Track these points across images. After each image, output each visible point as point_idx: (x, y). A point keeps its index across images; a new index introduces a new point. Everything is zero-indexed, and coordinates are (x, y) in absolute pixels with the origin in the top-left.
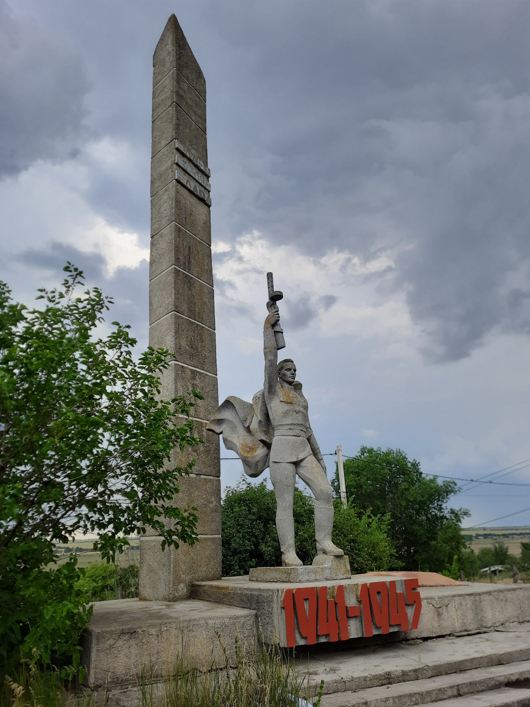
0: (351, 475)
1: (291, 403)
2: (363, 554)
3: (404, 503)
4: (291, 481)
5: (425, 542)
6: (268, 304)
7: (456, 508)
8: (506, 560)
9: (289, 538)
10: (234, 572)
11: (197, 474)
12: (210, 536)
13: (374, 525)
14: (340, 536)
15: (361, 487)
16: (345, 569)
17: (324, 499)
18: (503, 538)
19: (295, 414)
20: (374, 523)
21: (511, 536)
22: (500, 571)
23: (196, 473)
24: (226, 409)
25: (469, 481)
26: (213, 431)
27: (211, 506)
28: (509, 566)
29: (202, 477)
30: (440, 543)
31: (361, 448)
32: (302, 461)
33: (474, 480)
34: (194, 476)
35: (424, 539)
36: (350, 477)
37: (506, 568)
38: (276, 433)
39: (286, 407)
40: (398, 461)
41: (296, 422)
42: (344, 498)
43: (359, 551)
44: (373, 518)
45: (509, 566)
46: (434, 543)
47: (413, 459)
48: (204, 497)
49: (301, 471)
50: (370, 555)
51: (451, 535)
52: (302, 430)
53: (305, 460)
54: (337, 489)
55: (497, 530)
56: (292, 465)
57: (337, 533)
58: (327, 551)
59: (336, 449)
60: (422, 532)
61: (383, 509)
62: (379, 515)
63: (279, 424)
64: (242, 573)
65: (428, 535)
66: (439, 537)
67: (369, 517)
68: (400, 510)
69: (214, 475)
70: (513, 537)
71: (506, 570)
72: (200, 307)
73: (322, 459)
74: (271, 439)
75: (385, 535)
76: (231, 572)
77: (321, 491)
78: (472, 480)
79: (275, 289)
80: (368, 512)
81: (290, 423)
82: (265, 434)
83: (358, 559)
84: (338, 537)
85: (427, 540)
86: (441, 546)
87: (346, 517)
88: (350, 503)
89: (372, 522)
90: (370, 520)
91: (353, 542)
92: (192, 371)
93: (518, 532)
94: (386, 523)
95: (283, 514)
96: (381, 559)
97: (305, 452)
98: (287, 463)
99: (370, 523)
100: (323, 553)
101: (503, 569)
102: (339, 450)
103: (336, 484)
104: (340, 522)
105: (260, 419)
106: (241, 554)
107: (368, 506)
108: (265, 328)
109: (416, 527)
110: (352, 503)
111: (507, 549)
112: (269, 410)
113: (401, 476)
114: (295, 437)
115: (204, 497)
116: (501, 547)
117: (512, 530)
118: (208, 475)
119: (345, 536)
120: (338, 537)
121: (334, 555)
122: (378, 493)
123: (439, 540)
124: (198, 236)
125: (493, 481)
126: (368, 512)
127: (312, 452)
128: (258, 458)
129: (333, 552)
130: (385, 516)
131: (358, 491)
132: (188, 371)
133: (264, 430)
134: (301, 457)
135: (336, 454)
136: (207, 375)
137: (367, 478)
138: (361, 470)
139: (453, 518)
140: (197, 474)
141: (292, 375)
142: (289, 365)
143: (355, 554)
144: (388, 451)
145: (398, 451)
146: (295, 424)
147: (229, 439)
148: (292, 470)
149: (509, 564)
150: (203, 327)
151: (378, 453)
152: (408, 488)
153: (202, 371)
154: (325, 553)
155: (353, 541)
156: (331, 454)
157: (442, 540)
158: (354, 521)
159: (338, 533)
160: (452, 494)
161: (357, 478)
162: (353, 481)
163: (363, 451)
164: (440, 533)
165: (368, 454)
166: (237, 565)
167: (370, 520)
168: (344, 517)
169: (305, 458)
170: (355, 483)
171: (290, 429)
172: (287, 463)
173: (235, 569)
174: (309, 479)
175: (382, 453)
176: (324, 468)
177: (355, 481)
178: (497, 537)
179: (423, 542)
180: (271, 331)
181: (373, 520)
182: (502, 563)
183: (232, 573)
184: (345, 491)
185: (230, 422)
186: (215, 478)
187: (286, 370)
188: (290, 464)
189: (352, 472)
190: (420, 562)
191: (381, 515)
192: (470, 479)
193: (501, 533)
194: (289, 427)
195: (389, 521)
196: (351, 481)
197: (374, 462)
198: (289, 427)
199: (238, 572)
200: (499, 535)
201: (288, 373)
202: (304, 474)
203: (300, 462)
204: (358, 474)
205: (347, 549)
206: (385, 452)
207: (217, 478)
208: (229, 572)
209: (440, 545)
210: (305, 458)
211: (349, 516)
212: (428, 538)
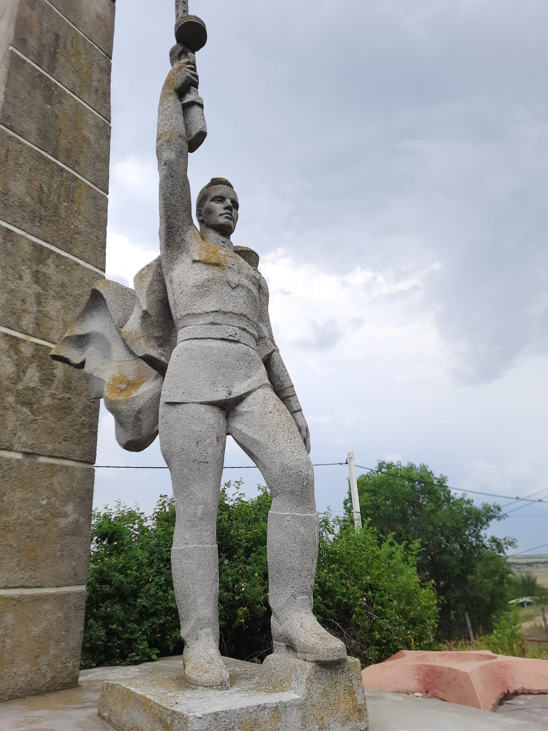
0: (366, 493)
1: (217, 265)
2: (390, 612)
3: (430, 528)
4: (210, 451)
5: (458, 575)
6: (172, 53)
7: (500, 536)
8: (535, 592)
9: (201, 600)
10: (137, 655)
11: (26, 454)
12: (52, 591)
13: (399, 555)
14: (347, 578)
15: (378, 508)
16: (350, 705)
17: (292, 492)
18: (527, 567)
19: (227, 289)
20: (398, 552)
21: (534, 565)
22: (529, 604)
23: (23, 449)
24: (95, 313)
25: (514, 498)
26: (65, 360)
27: (63, 522)
28: (538, 598)
29: (42, 460)
30: (480, 578)
31: (378, 463)
32: (240, 399)
33: (520, 498)
34: (19, 456)
35: (457, 571)
36: (365, 496)
37: (534, 600)
38: (181, 334)
39: (205, 273)
40: (421, 477)
41: (230, 308)
42: (358, 520)
43: (383, 606)
44: (397, 545)
45: (538, 598)
46: (470, 577)
47: (440, 474)
48: (44, 503)
49: (239, 424)
50: (402, 613)
51: (493, 567)
52: (244, 330)
53: (249, 399)
54: (349, 510)
55: (520, 558)
56: (216, 410)
57: (341, 574)
58: (296, 643)
59: (347, 457)
60: (454, 563)
61: (406, 535)
62: (404, 543)
63: (185, 313)
64: (154, 657)
65: (461, 566)
66: (478, 570)
67: (392, 544)
68: (427, 537)
69: (77, 458)
70: (537, 566)
71: (535, 602)
72: (72, 141)
73: (300, 410)
74: (168, 356)
75: (415, 569)
76: (130, 655)
77: (284, 468)
78: (518, 498)
79: (191, 12)
80: (390, 537)
81: (213, 309)
82: (159, 346)
83: (380, 622)
84: (344, 581)
85: (460, 573)
86: (481, 582)
87: (358, 544)
88: (366, 526)
89: (396, 551)
90: (394, 549)
91: (372, 590)
92: (34, 244)
93: (543, 560)
94: (414, 553)
95: (187, 537)
96: (423, 622)
97: (250, 381)
98: (202, 403)
99: (393, 553)
100: (288, 647)
101: (531, 601)
102: (351, 458)
103: (348, 505)
104: (349, 553)
105: (145, 308)
106: (157, 616)
107: (387, 532)
108: (164, 96)
109: (446, 557)
110: (369, 525)
111: (535, 579)
112: (168, 285)
113: (426, 495)
114: (225, 343)
115: (44, 503)
116: (529, 578)
117: (536, 558)
118: (62, 458)
119: (357, 578)
120: (344, 581)
121: (317, 662)
122: (399, 516)
123: (479, 574)
124: (81, 30)
125: (544, 500)
126: (390, 537)
127: (267, 381)
128: (141, 402)
129: (312, 650)
130: (412, 543)
131: (375, 513)
132: (22, 243)
133: (156, 335)
134: (238, 390)
135: (347, 463)
136: (78, 264)
137: (386, 497)
138: (378, 487)
139: (494, 547)
140: (26, 454)
141: (227, 211)
142: (221, 190)
143: (376, 613)
144: (409, 466)
145: (422, 466)
146: (225, 313)
147: (95, 375)
148: (212, 422)
149: (538, 596)
150: (77, 178)
151: (398, 469)
152: (435, 510)
153: (63, 253)
154: (291, 647)
155: (371, 587)
156: (341, 464)
157: (482, 574)
158: (372, 551)
159: (344, 573)
160: (494, 520)
161: (373, 497)
162: (369, 501)
163: (381, 465)
164: (478, 565)
165: (386, 470)
166: (144, 640)
167: (394, 549)
168: (356, 544)
169: (248, 394)
170: (371, 503)
171: (213, 324)
172: (202, 403)
173: (139, 650)
174: (255, 442)
175: (402, 469)
176: (304, 433)
177: (371, 501)
178: (520, 566)
179: (456, 575)
180: (174, 103)
181: (397, 549)
182: (530, 594)
183: (133, 657)
184: (359, 511)
185: (100, 337)
186: (80, 465)
187: (213, 200)
188: (208, 407)
189: (367, 491)
190: (453, 600)
191: (407, 542)
192: (514, 497)
193: (524, 561)
194: (210, 319)
195: (419, 551)
196: (366, 501)
197: (394, 476)
198: (210, 319)
199: (144, 654)
200: (522, 564)
201: (219, 208)
202: (244, 431)
203: (237, 404)
204: (374, 492)
205: (361, 605)
206: (406, 468)
207: (86, 466)
208: (127, 656)
209: (480, 580)
210: (248, 394)
211: (364, 543)
212: (462, 570)
